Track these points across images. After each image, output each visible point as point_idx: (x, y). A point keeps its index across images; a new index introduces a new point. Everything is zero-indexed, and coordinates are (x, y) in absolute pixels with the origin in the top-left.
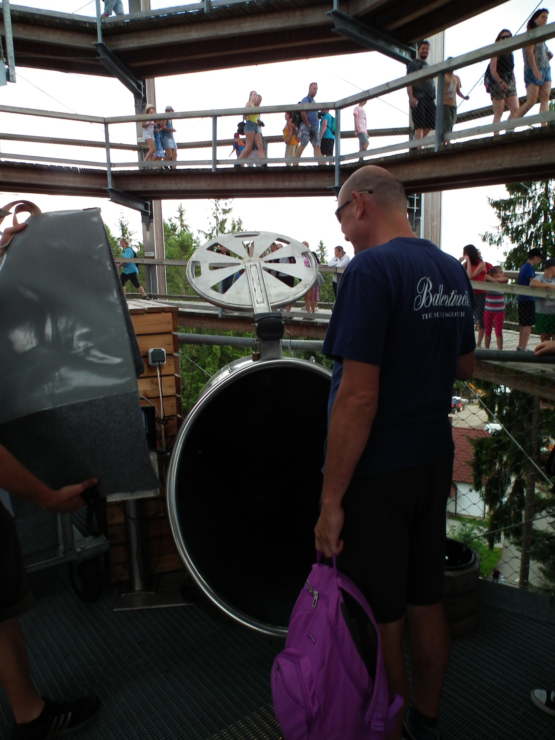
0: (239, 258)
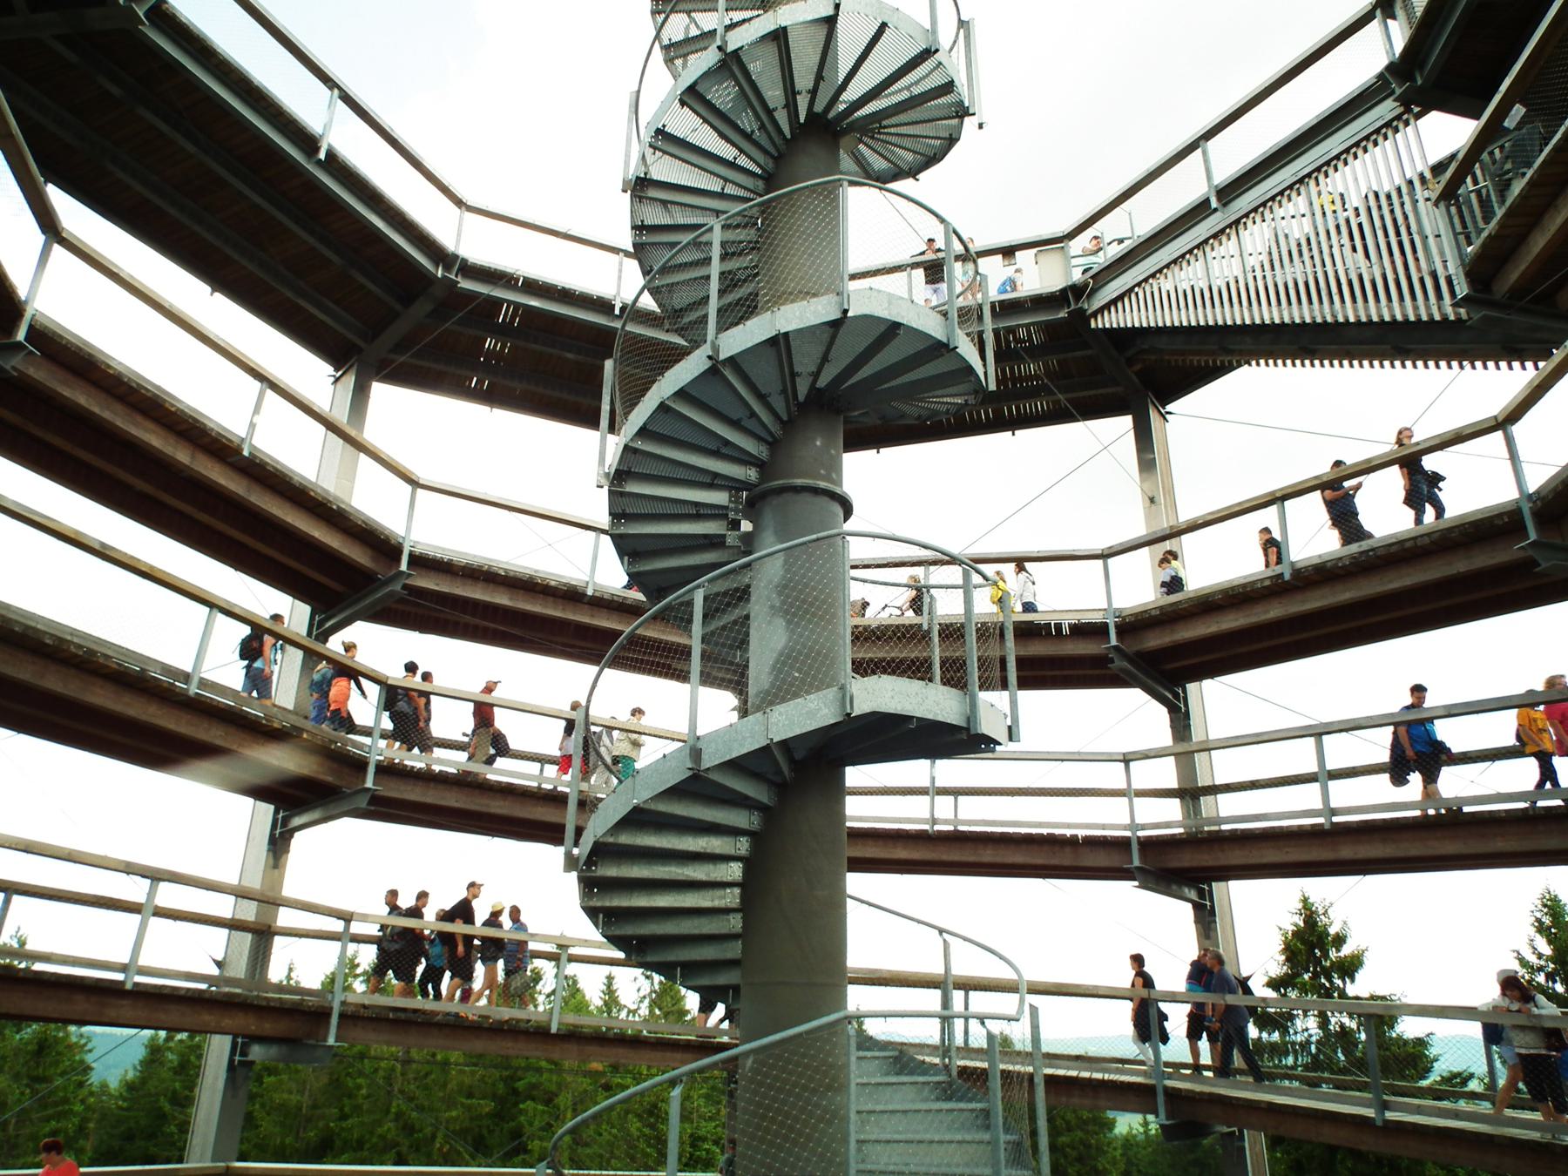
0: (1350, 967)
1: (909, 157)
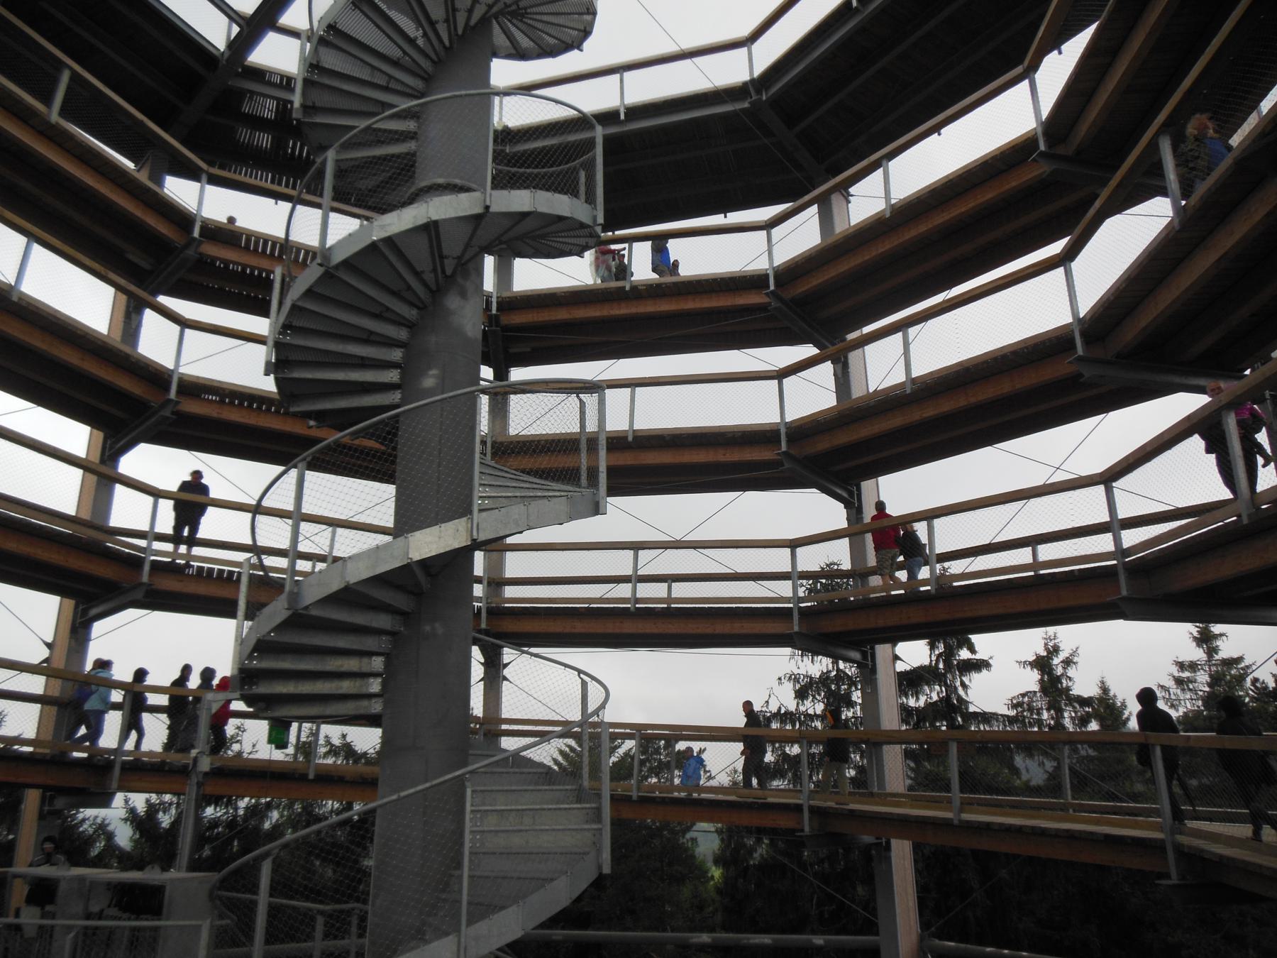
1: (552, 41)
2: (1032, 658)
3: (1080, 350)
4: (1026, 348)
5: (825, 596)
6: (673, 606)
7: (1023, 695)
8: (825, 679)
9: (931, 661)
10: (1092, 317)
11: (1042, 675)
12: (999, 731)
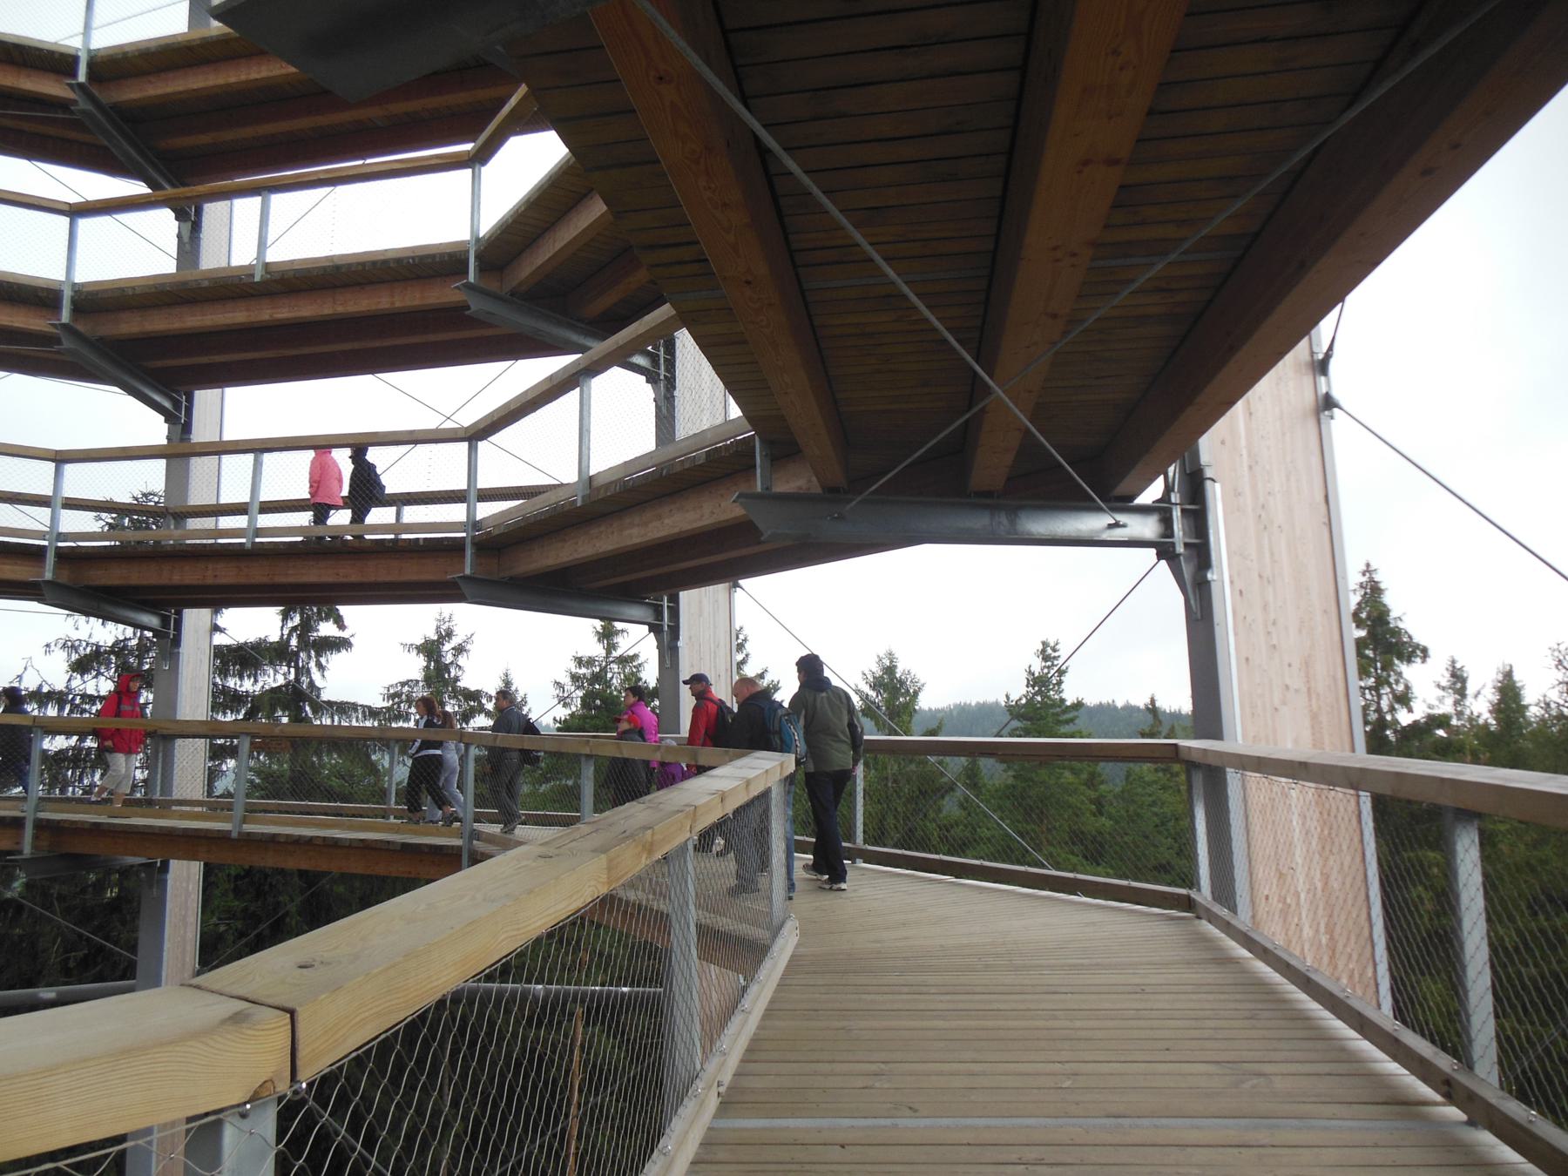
2: (420, 641)
3: (471, 277)
4: (413, 258)
5: (133, 536)
6: (404, 536)
7: (403, 684)
8: (119, 649)
9: (282, 635)
10: (490, 237)
11: (429, 662)
12: (332, 726)
